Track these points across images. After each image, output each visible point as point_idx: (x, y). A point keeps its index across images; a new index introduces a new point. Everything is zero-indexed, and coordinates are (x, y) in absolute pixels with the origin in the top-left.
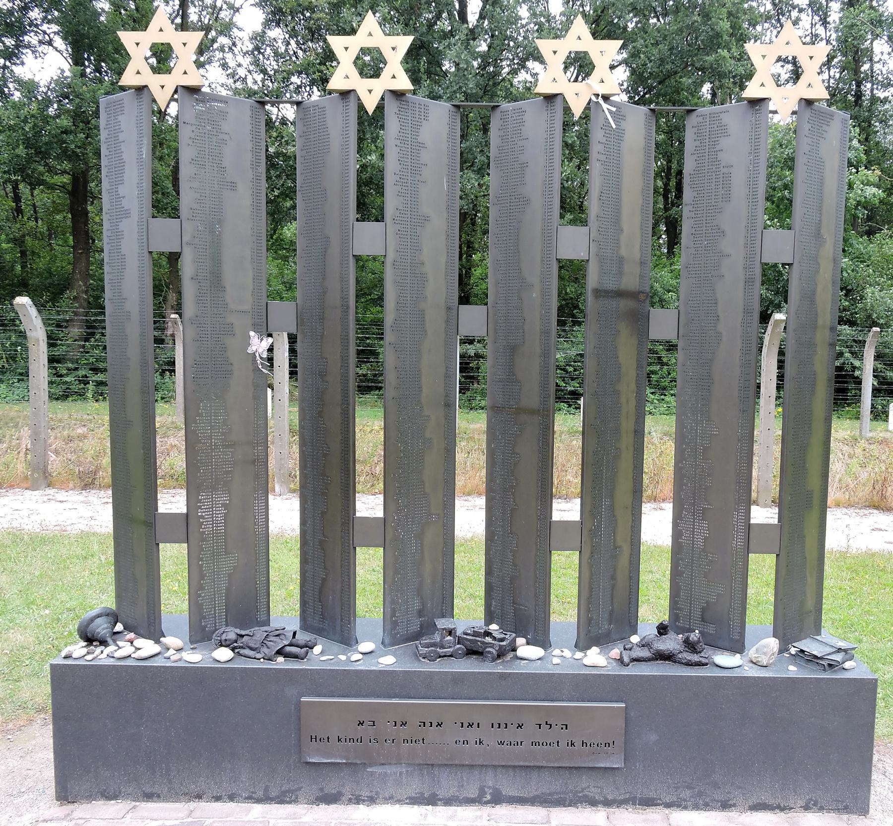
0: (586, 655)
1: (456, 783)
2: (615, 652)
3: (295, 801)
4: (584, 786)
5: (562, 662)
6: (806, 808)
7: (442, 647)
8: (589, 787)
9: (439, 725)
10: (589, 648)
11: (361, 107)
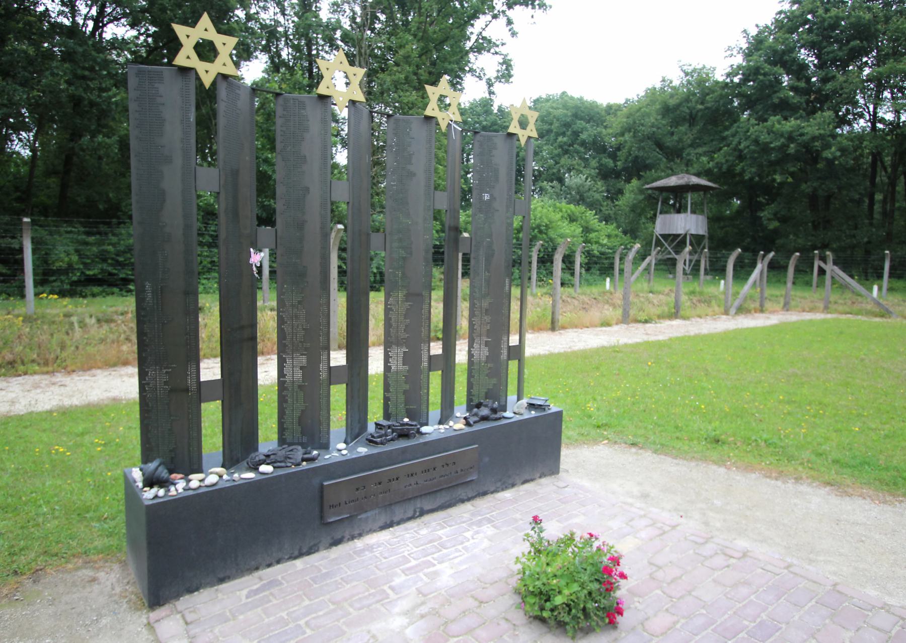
3: (317, 551)
6: (540, 477)
11: (201, 84)
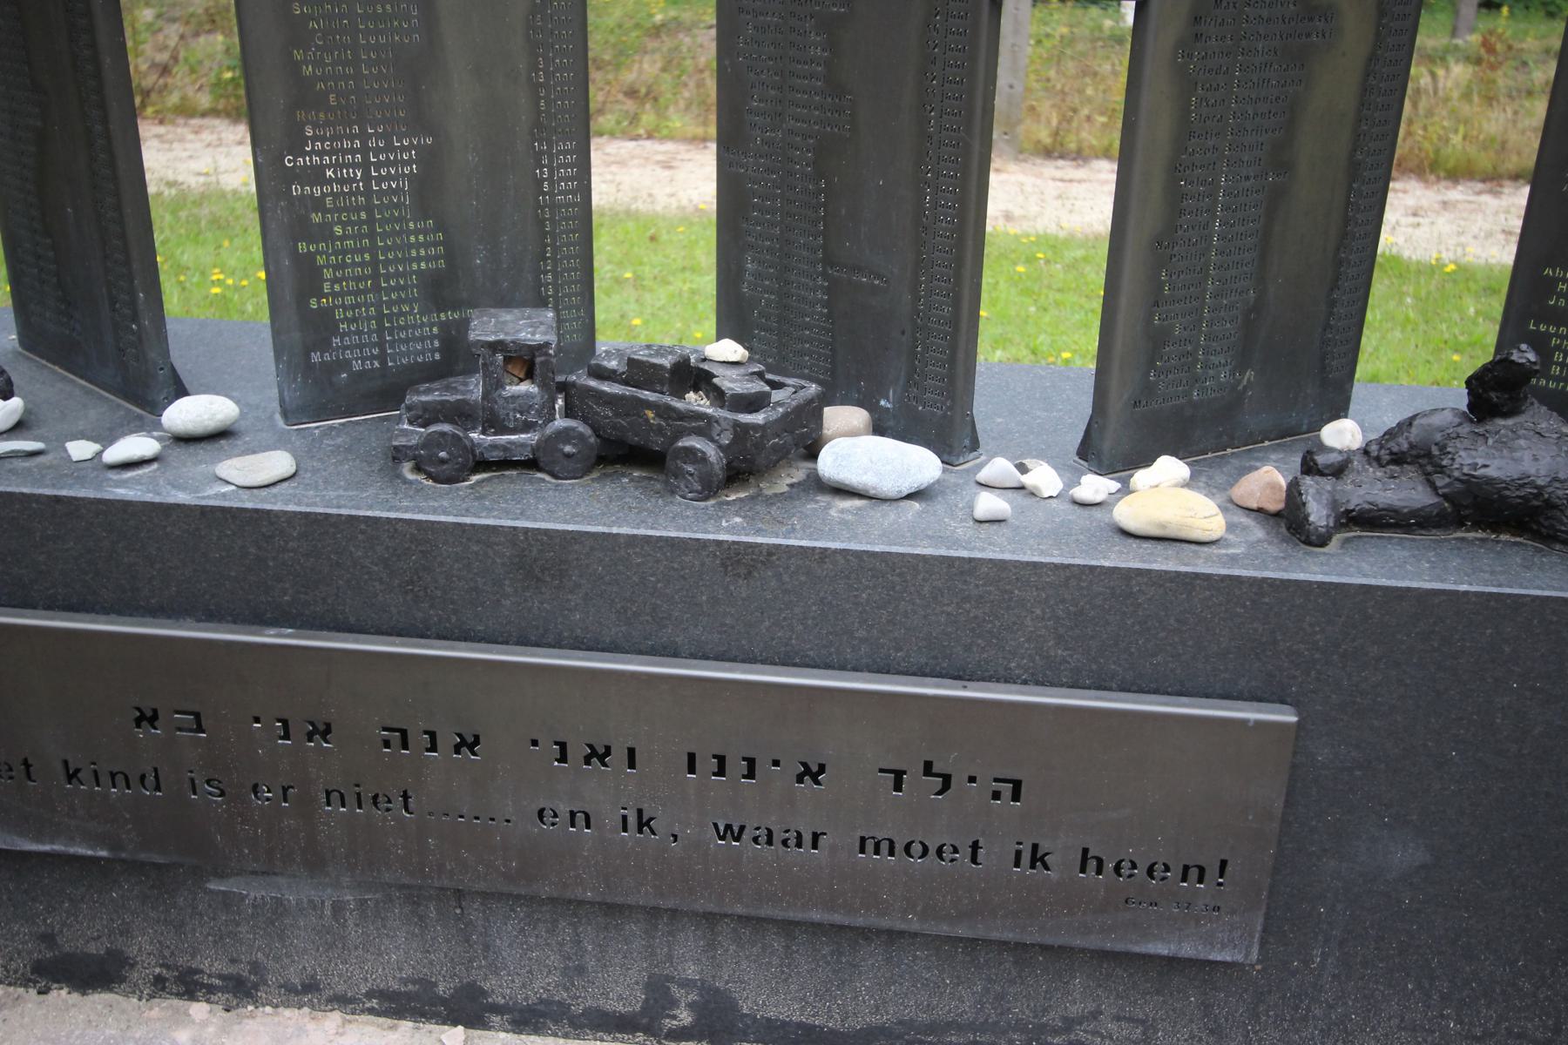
0: (1126, 490)
1: (554, 959)
2: (1267, 480)
4: (1074, 1010)
5: (1019, 511)
7: (494, 424)
8: (1095, 1015)
9: (469, 743)
10: (1146, 460)
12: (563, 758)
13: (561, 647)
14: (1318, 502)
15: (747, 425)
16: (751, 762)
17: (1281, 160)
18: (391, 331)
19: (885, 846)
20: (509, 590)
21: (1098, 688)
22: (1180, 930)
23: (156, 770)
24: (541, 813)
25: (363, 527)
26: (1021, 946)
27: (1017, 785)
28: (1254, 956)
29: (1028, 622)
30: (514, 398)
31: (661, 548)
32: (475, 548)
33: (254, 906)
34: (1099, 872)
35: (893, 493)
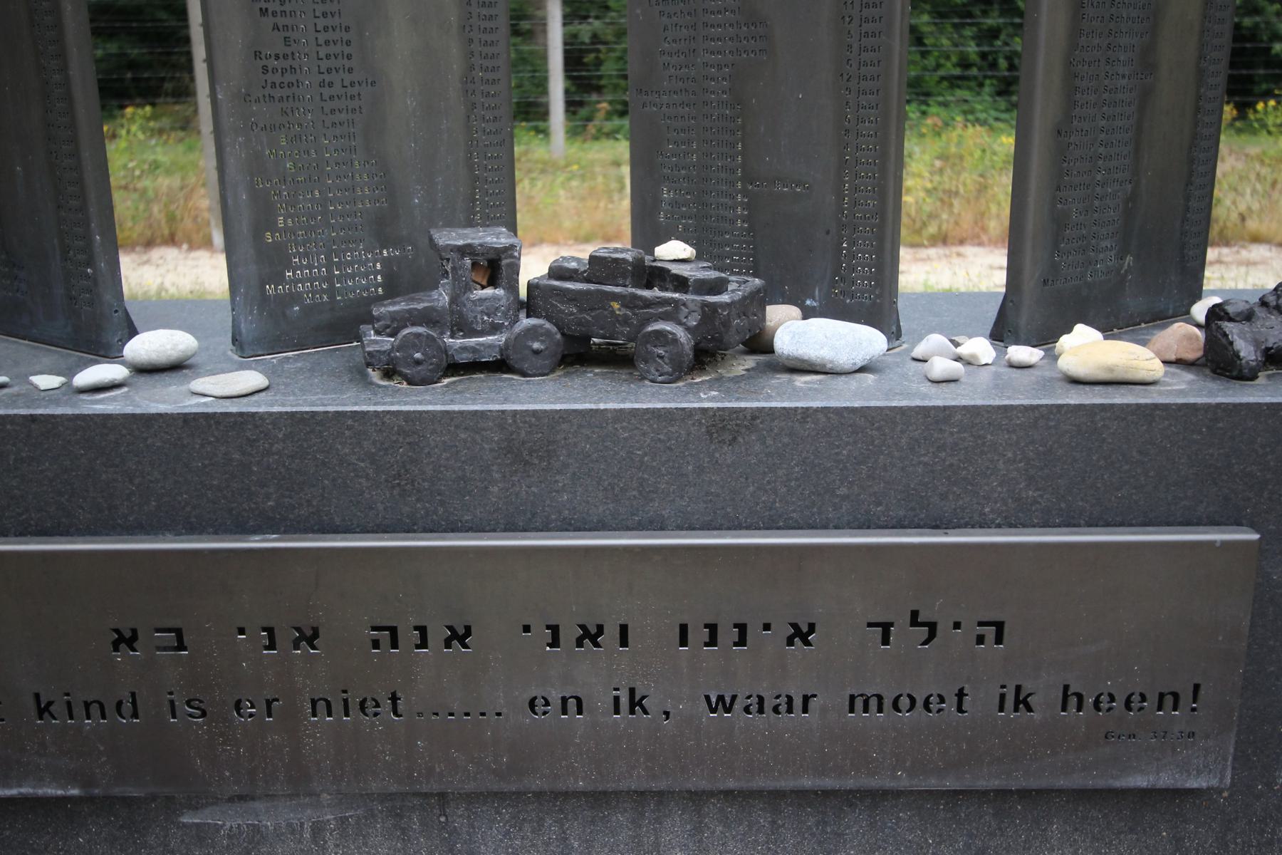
7: (463, 327)
9: (459, 636)
12: (555, 643)
13: (549, 530)
14: (1245, 339)
15: (714, 303)
16: (742, 628)
17: (1147, 63)
18: (339, 266)
19: (873, 703)
20: (497, 476)
21: (1068, 525)
22: (1158, 759)
23: (133, 695)
24: (532, 704)
25: (350, 422)
26: (1002, 794)
27: (999, 626)
28: (1228, 781)
29: (1001, 465)
30: (482, 300)
31: (647, 421)
32: (463, 436)
33: (230, 837)
34: (1079, 709)
35: (848, 367)
